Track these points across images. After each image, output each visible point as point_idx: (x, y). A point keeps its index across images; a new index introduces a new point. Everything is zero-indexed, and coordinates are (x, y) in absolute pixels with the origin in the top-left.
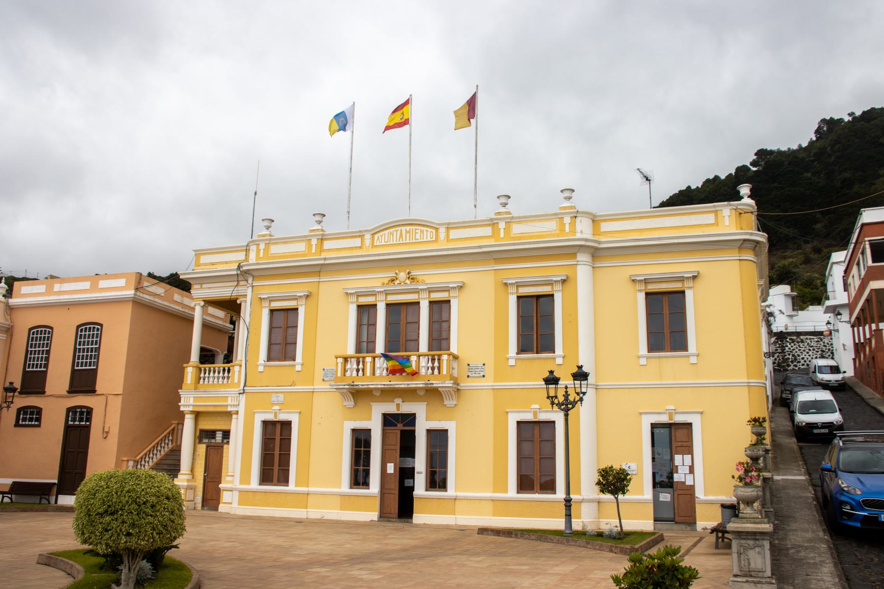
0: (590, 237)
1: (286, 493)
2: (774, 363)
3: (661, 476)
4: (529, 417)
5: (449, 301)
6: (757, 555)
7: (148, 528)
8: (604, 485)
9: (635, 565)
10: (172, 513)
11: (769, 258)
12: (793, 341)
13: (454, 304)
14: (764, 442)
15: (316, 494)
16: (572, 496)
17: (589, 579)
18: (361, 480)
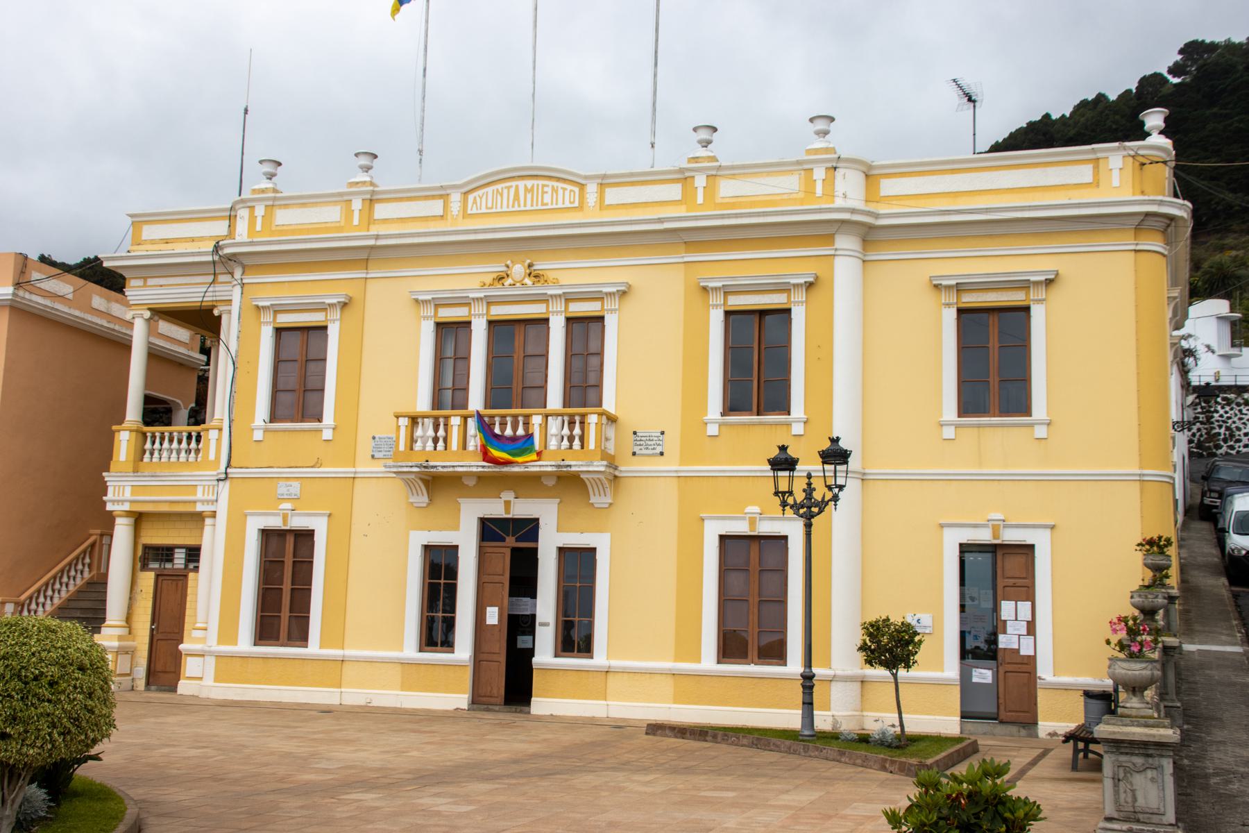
0: (860, 205)
1: (304, 659)
2: (1190, 442)
3: (976, 637)
4: (741, 528)
5: (601, 319)
6: (1150, 785)
7: (44, 725)
8: (873, 652)
9: (927, 792)
10: (90, 695)
11: (1192, 248)
12: (1229, 402)
13: (611, 323)
14: (1167, 581)
15: (357, 660)
16: (815, 670)
17: (844, 817)
18: (439, 637)
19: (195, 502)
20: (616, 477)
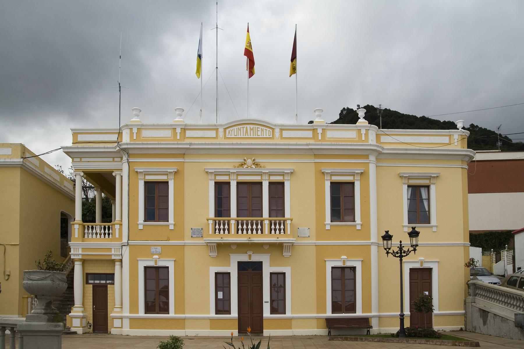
15: (191, 318)
19: (111, 255)
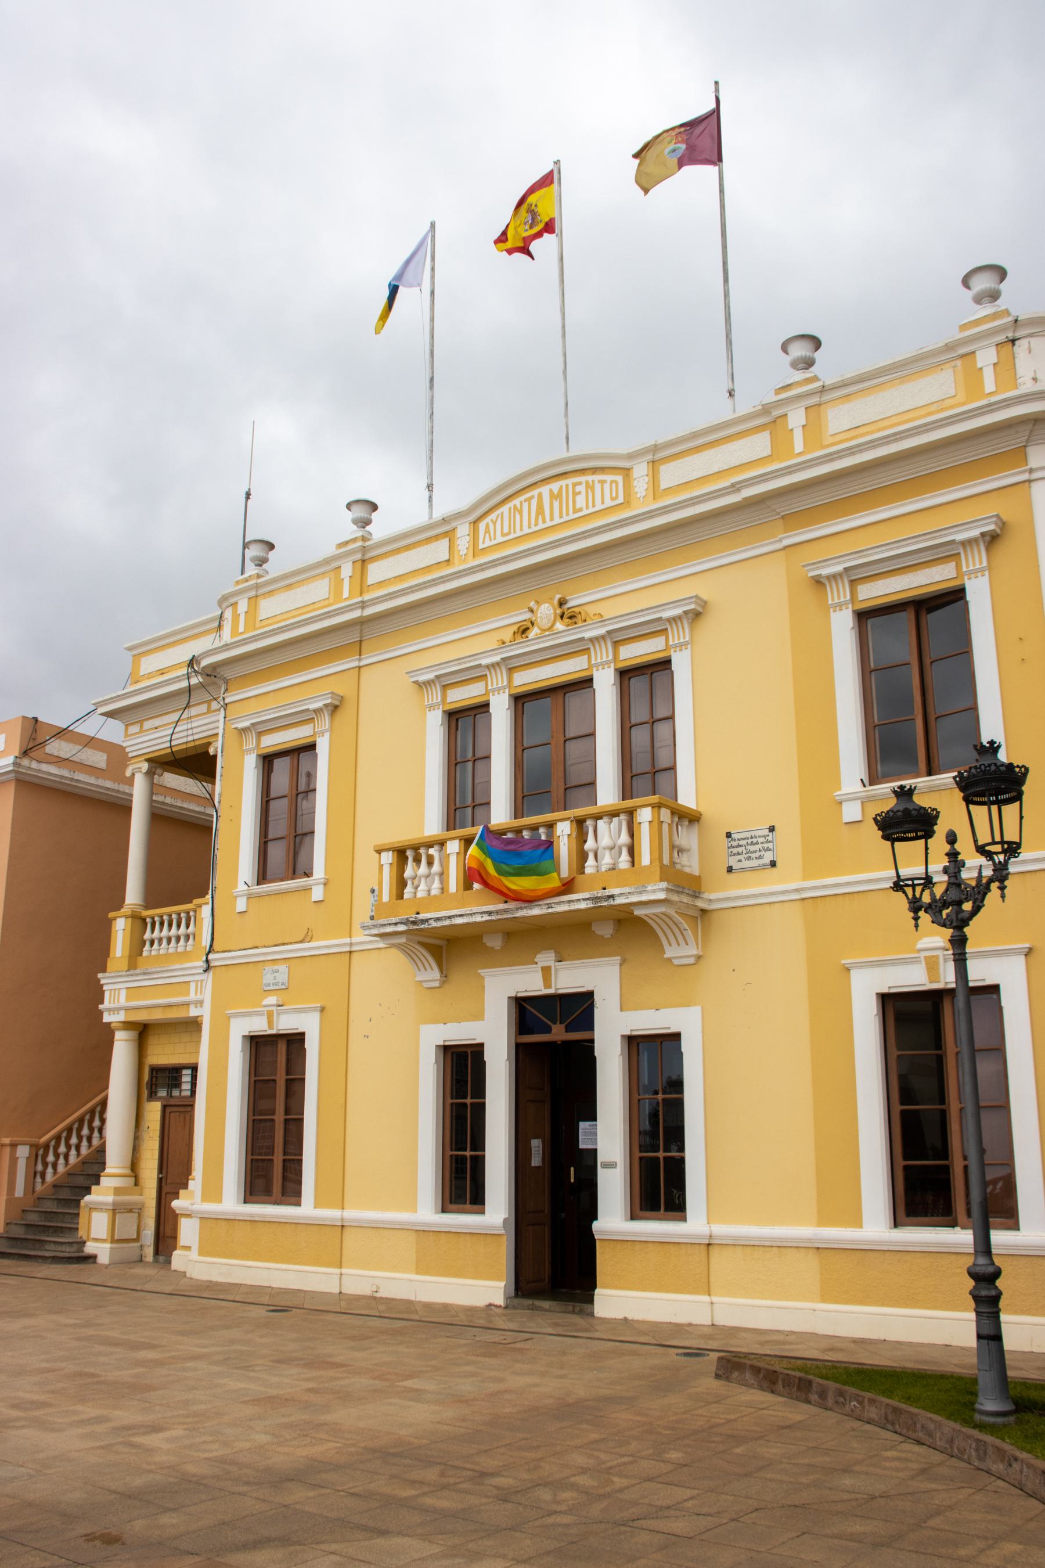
15: (376, 1227)
19: (187, 1004)
20: (703, 911)
